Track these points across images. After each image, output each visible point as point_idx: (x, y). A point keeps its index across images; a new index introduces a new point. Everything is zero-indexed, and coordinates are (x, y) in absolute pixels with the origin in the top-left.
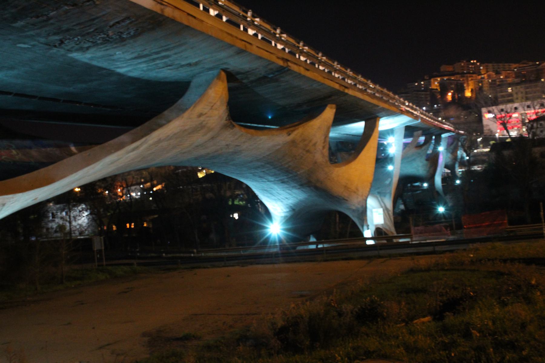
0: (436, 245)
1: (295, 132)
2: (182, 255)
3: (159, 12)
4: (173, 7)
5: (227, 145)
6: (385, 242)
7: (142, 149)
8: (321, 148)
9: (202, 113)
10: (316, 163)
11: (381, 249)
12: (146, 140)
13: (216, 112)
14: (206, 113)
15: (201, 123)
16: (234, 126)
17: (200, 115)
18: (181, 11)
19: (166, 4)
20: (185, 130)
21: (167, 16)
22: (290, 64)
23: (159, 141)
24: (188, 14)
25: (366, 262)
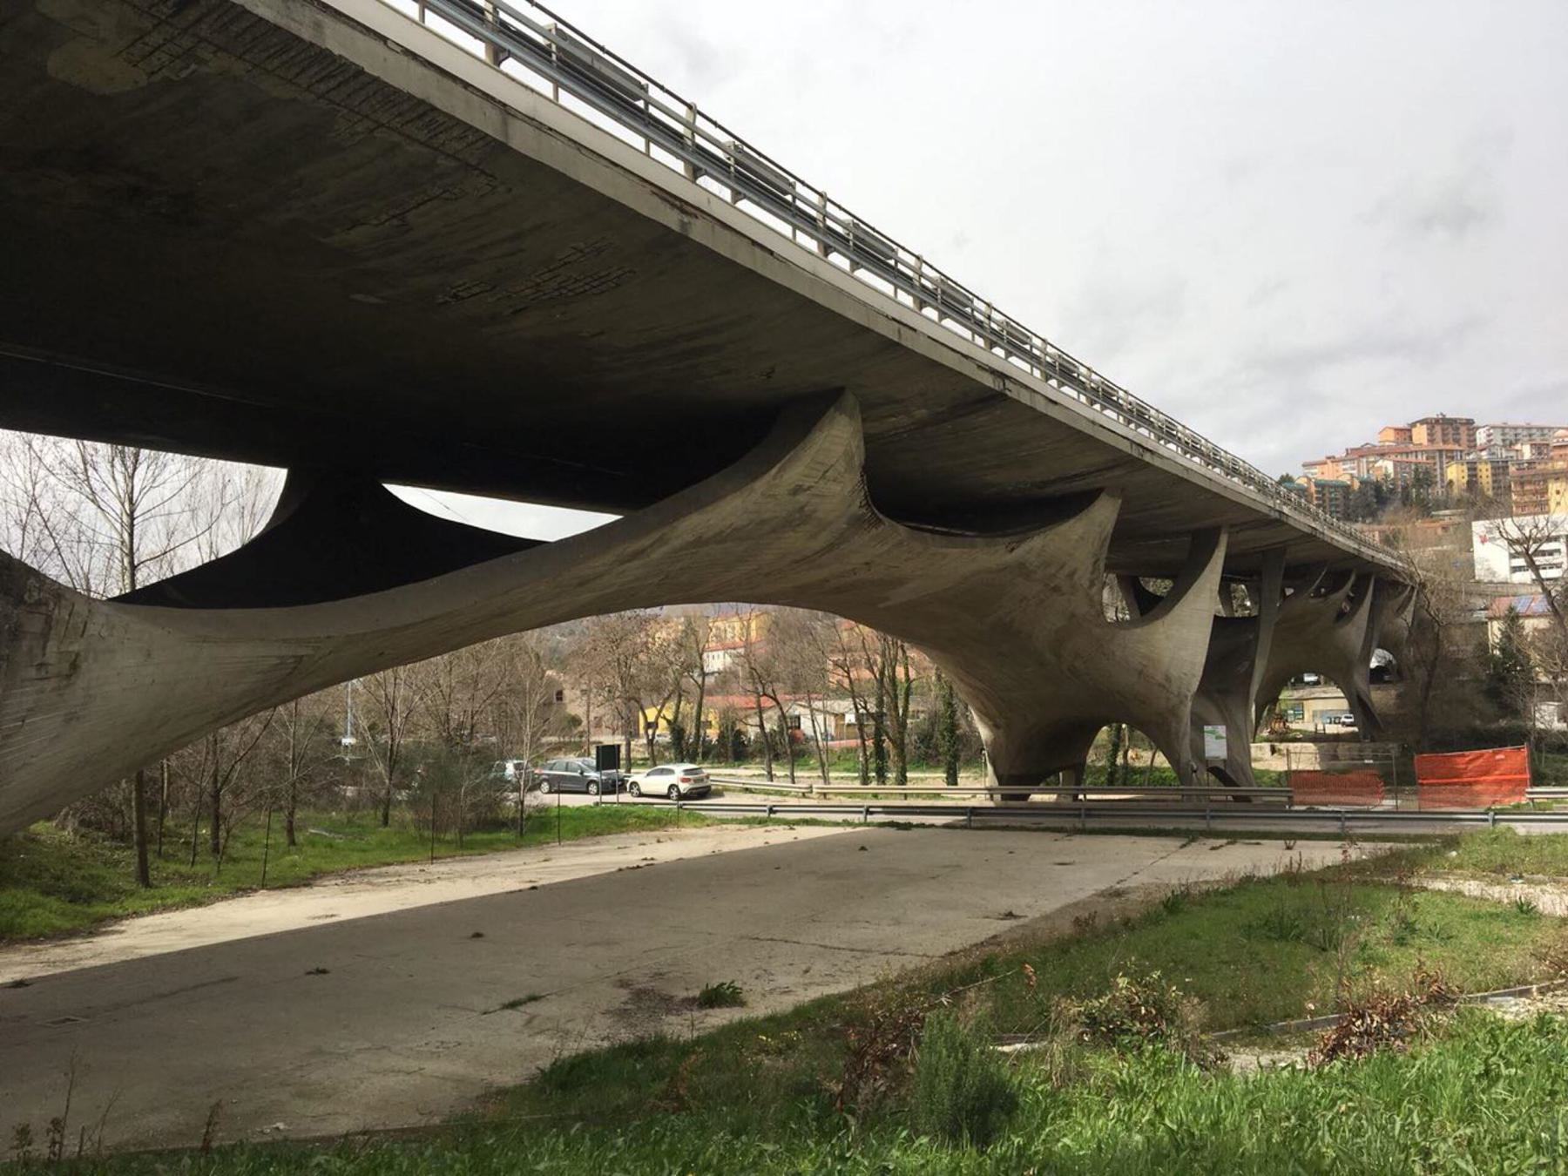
0: (770, 794)
1: (1025, 547)
2: (166, 785)
3: (675, 227)
4: (566, 141)
5: (867, 564)
6: (1036, 798)
7: (656, 555)
8: (1086, 584)
9: (801, 486)
10: (1073, 615)
11: (1088, 816)
12: (661, 538)
13: (837, 488)
14: (809, 488)
15: (802, 508)
16: (880, 521)
17: (797, 490)
18: (742, 238)
19: (692, 210)
20: (763, 522)
21: (419, 96)
22: (1009, 385)
23: (699, 542)
24: (754, 243)
25: (1178, 843)
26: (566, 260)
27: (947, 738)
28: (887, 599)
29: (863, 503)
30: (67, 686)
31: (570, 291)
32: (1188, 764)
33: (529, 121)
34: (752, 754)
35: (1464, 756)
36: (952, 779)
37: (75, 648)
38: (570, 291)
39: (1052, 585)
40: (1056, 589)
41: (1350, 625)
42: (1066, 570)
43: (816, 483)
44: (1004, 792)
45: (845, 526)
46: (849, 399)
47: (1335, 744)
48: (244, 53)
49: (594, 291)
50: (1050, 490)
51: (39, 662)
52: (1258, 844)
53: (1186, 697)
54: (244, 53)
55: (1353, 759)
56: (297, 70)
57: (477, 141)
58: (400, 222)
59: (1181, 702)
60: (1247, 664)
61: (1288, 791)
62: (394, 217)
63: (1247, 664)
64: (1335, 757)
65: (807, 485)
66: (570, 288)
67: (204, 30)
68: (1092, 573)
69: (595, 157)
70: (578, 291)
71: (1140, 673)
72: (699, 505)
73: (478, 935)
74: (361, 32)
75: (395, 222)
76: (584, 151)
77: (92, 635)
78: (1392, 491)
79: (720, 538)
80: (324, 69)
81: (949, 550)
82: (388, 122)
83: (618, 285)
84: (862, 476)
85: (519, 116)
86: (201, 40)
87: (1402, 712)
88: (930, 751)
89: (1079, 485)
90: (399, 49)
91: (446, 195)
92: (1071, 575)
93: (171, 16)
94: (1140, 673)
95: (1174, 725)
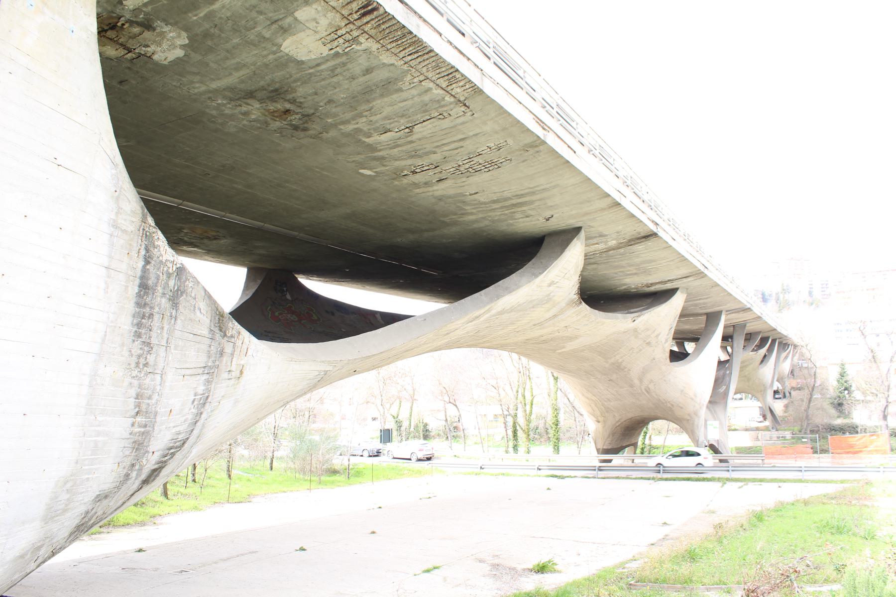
8: (663, 342)
15: (549, 295)
20: (532, 301)
23: (501, 313)
26: (480, 153)
27: (554, 429)
28: (564, 347)
29: (576, 292)
30: (237, 384)
31: (473, 169)
32: (703, 442)
33: (489, 78)
34: (433, 436)
35: (854, 437)
36: (557, 449)
37: (242, 362)
38: (473, 169)
39: (647, 341)
40: (649, 344)
41: (766, 367)
42: (656, 333)
43: (560, 280)
44: (599, 458)
45: (564, 305)
46: (582, 234)
47: (758, 432)
48: (380, 40)
49: (486, 170)
50: (653, 289)
51: (229, 370)
52: (761, 485)
53: (703, 405)
54: (380, 40)
55: (767, 440)
56: (401, 49)
57: (469, 88)
58: (410, 131)
59: (701, 408)
60: (724, 387)
61: (762, 457)
62: (407, 128)
63: (724, 387)
64: (757, 439)
65: (556, 281)
66: (474, 168)
67: (367, 28)
68: (668, 335)
69: (514, 99)
70: (476, 170)
71: (682, 391)
72: (509, 290)
73: (373, 533)
74: (432, 30)
75: (407, 130)
76: (510, 95)
77: (250, 355)
78: (770, 295)
79: (512, 310)
80: (415, 49)
81: (605, 320)
82: (431, 77)
83: (499, 167)
84: (580, 277)
85: (487, 76)
86: (365, 32)
87: (786, 414)
88: (536, 436)
89: (669, 286)
90: (446, 40)
91: (440, 117)
92: (657, 336)
93: (356, 20)
94: (682, 391)
95: (696, 420)
